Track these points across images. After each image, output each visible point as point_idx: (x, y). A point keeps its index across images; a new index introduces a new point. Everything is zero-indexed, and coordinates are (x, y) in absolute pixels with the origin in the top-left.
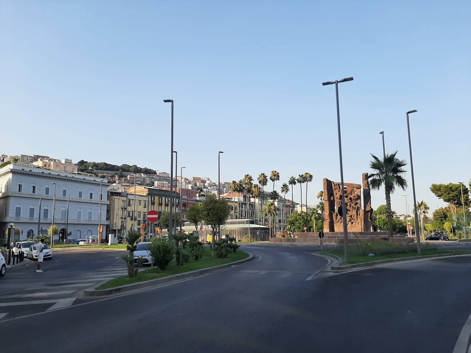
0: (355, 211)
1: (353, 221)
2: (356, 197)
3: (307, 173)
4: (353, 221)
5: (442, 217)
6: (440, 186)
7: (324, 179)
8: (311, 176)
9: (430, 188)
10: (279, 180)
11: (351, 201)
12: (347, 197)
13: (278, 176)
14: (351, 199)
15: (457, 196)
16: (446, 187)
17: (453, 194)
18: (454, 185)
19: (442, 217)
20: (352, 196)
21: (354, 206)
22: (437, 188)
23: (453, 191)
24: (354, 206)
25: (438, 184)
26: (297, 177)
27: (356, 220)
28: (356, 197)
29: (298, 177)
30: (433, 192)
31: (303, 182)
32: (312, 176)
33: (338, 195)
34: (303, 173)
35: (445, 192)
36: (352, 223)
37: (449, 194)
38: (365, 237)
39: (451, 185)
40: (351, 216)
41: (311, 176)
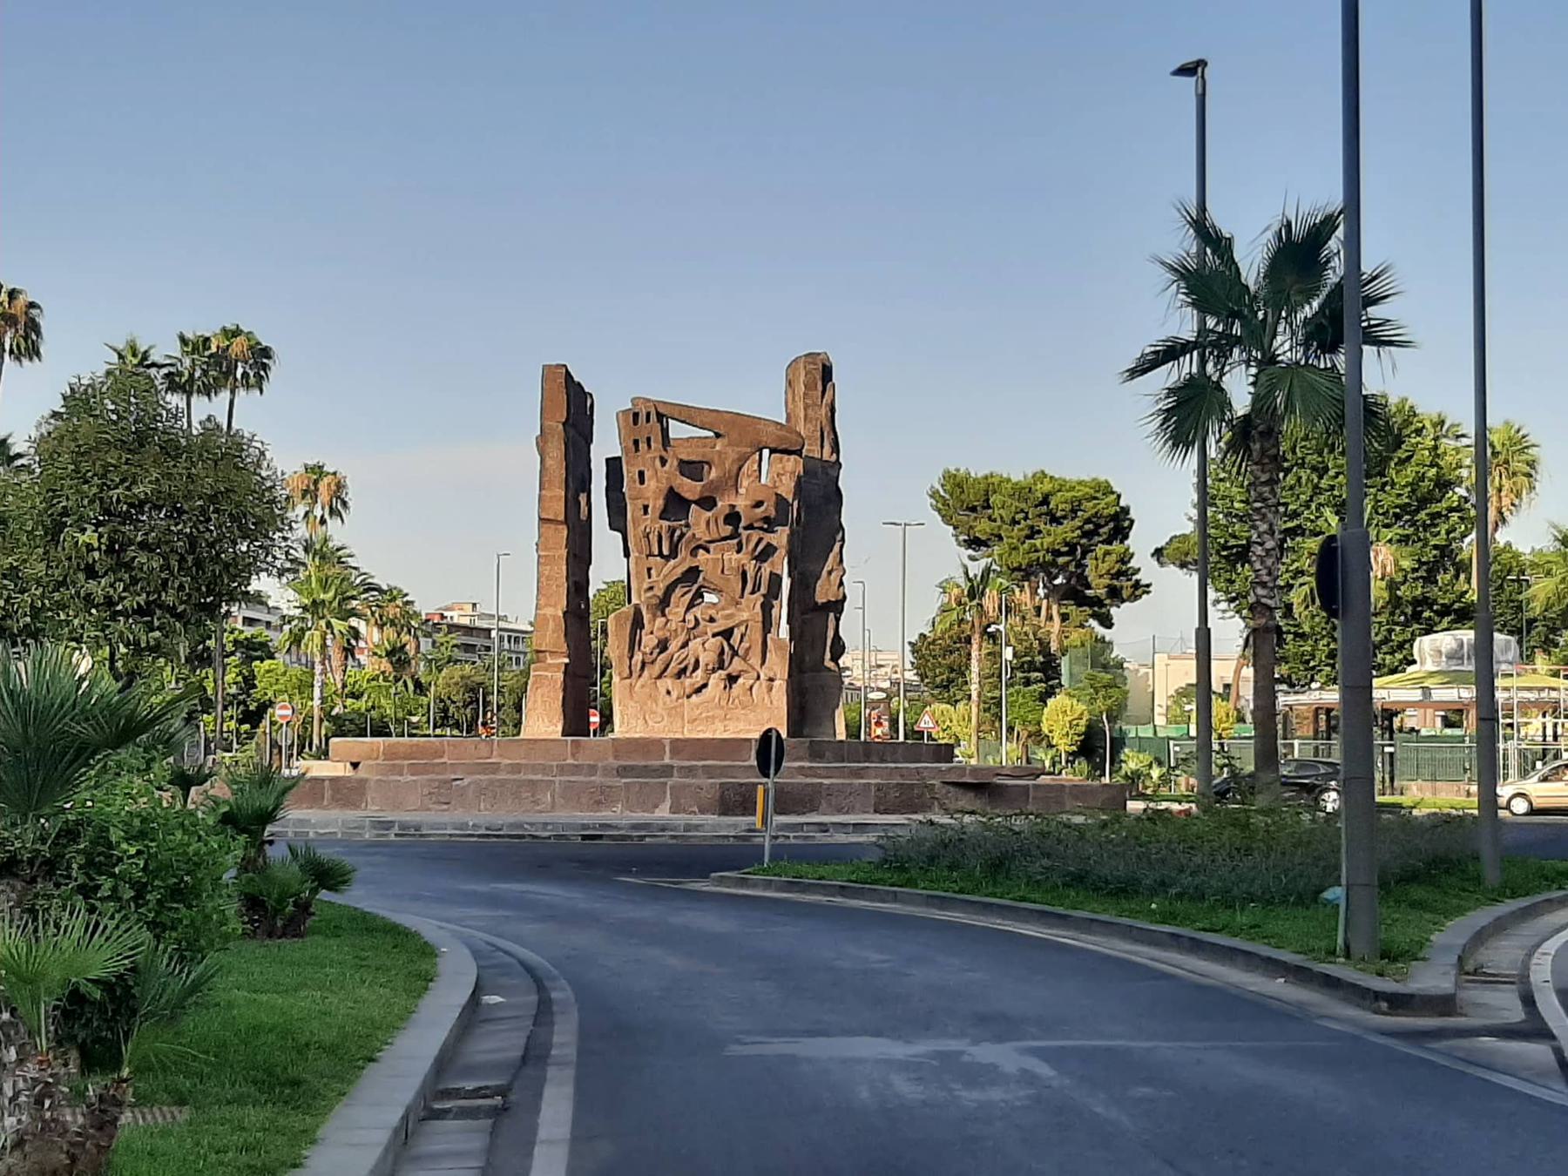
0: (758, 599)
1: (736, 665)
2: (769, 509)
3: (236, 333)
4: (736, 665)
5: (1032, 667)
6: (990, 486)
7: (548, 371)
8: (261, 356)
9: (934, 494)
10: (34, 352)
11: (735, 535)
12: (707, 502)
13: (33, 326)
14: (733, 518)
15: (1072, 548)
16: (1021, 492)
17: (1054, 536)
18: (1062, 486)
19: (1032, 667)
20: (741, 504)
21: (751, 568)
22: (972, 498)
23: (1055, 520)
24: (751, 568)
25: (978, 471)
26: (165, 349)
27: (755, 660)
28: (769, 509)
29: (176, 350)
30: (947, 519)
31: (207, 391)
32: (266, 352)
33: (651, 484)
34: (207, 325)
35: (1014, 522)
36: (732, 679)
37: (1033, 533)
38: (857, 773)
39: (1047, 487)
40: (727, 634)
41: (261, 356)
